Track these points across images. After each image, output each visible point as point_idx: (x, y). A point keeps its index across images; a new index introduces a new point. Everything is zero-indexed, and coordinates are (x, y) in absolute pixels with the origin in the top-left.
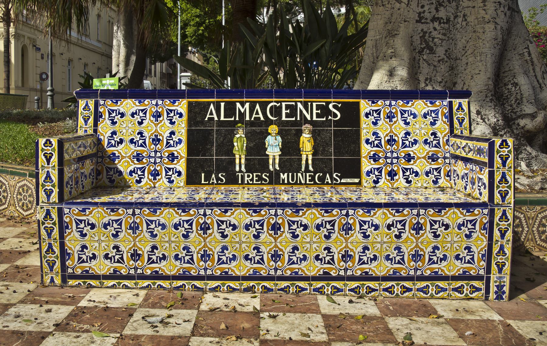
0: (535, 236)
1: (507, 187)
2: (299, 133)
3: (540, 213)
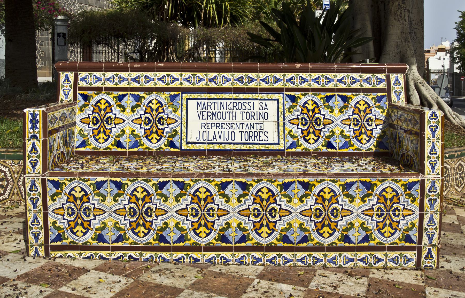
0: (11, 176)
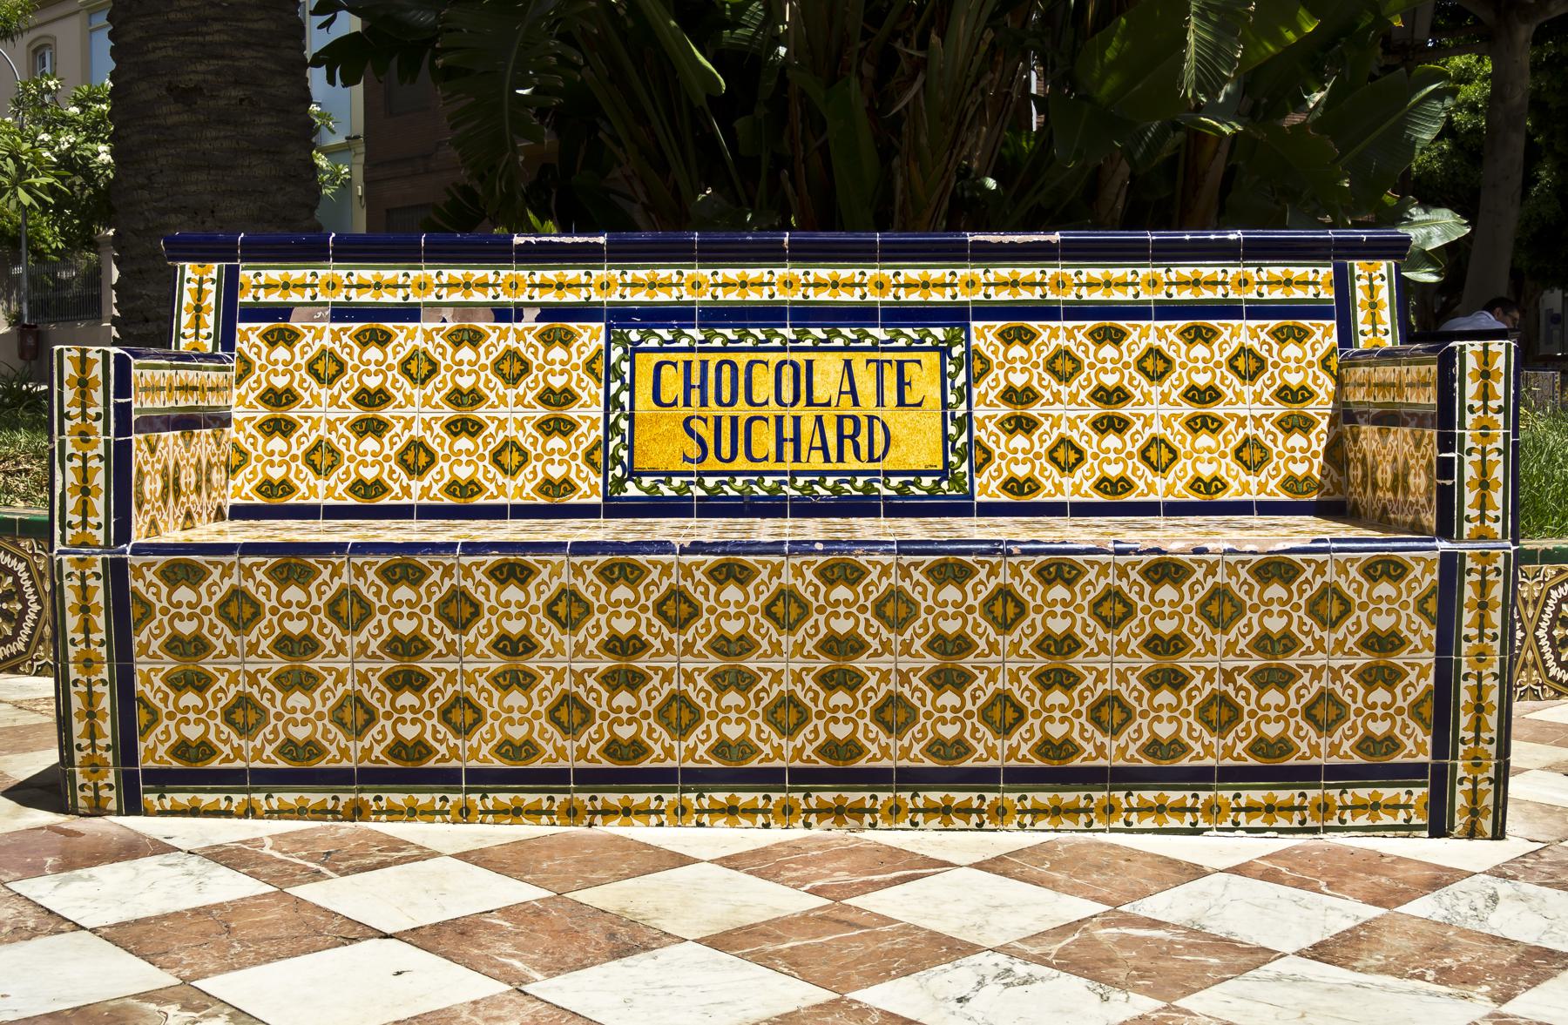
0: (1542, 655)
3: (1555, 588)
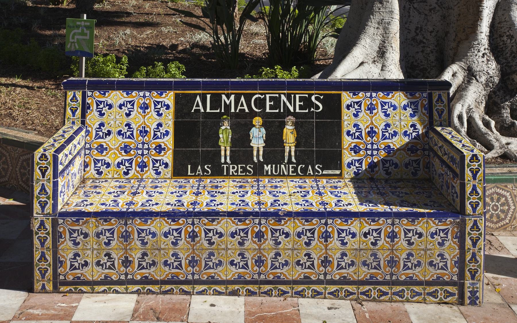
1: (478, 199)
2: (283, 125)
